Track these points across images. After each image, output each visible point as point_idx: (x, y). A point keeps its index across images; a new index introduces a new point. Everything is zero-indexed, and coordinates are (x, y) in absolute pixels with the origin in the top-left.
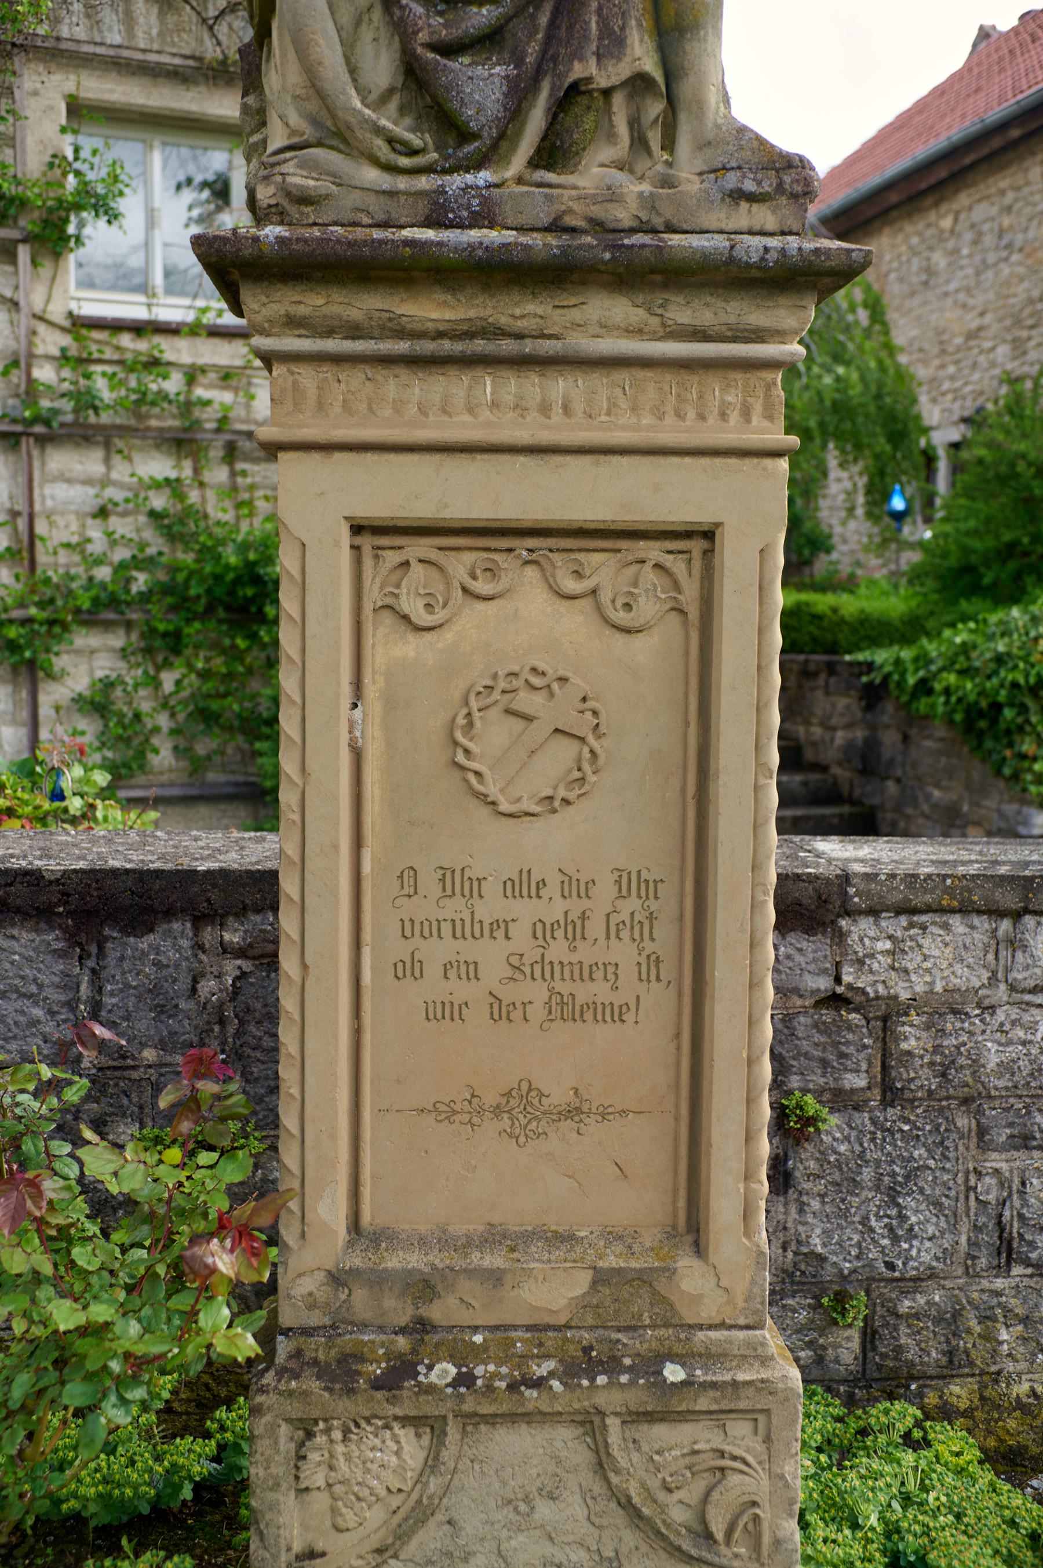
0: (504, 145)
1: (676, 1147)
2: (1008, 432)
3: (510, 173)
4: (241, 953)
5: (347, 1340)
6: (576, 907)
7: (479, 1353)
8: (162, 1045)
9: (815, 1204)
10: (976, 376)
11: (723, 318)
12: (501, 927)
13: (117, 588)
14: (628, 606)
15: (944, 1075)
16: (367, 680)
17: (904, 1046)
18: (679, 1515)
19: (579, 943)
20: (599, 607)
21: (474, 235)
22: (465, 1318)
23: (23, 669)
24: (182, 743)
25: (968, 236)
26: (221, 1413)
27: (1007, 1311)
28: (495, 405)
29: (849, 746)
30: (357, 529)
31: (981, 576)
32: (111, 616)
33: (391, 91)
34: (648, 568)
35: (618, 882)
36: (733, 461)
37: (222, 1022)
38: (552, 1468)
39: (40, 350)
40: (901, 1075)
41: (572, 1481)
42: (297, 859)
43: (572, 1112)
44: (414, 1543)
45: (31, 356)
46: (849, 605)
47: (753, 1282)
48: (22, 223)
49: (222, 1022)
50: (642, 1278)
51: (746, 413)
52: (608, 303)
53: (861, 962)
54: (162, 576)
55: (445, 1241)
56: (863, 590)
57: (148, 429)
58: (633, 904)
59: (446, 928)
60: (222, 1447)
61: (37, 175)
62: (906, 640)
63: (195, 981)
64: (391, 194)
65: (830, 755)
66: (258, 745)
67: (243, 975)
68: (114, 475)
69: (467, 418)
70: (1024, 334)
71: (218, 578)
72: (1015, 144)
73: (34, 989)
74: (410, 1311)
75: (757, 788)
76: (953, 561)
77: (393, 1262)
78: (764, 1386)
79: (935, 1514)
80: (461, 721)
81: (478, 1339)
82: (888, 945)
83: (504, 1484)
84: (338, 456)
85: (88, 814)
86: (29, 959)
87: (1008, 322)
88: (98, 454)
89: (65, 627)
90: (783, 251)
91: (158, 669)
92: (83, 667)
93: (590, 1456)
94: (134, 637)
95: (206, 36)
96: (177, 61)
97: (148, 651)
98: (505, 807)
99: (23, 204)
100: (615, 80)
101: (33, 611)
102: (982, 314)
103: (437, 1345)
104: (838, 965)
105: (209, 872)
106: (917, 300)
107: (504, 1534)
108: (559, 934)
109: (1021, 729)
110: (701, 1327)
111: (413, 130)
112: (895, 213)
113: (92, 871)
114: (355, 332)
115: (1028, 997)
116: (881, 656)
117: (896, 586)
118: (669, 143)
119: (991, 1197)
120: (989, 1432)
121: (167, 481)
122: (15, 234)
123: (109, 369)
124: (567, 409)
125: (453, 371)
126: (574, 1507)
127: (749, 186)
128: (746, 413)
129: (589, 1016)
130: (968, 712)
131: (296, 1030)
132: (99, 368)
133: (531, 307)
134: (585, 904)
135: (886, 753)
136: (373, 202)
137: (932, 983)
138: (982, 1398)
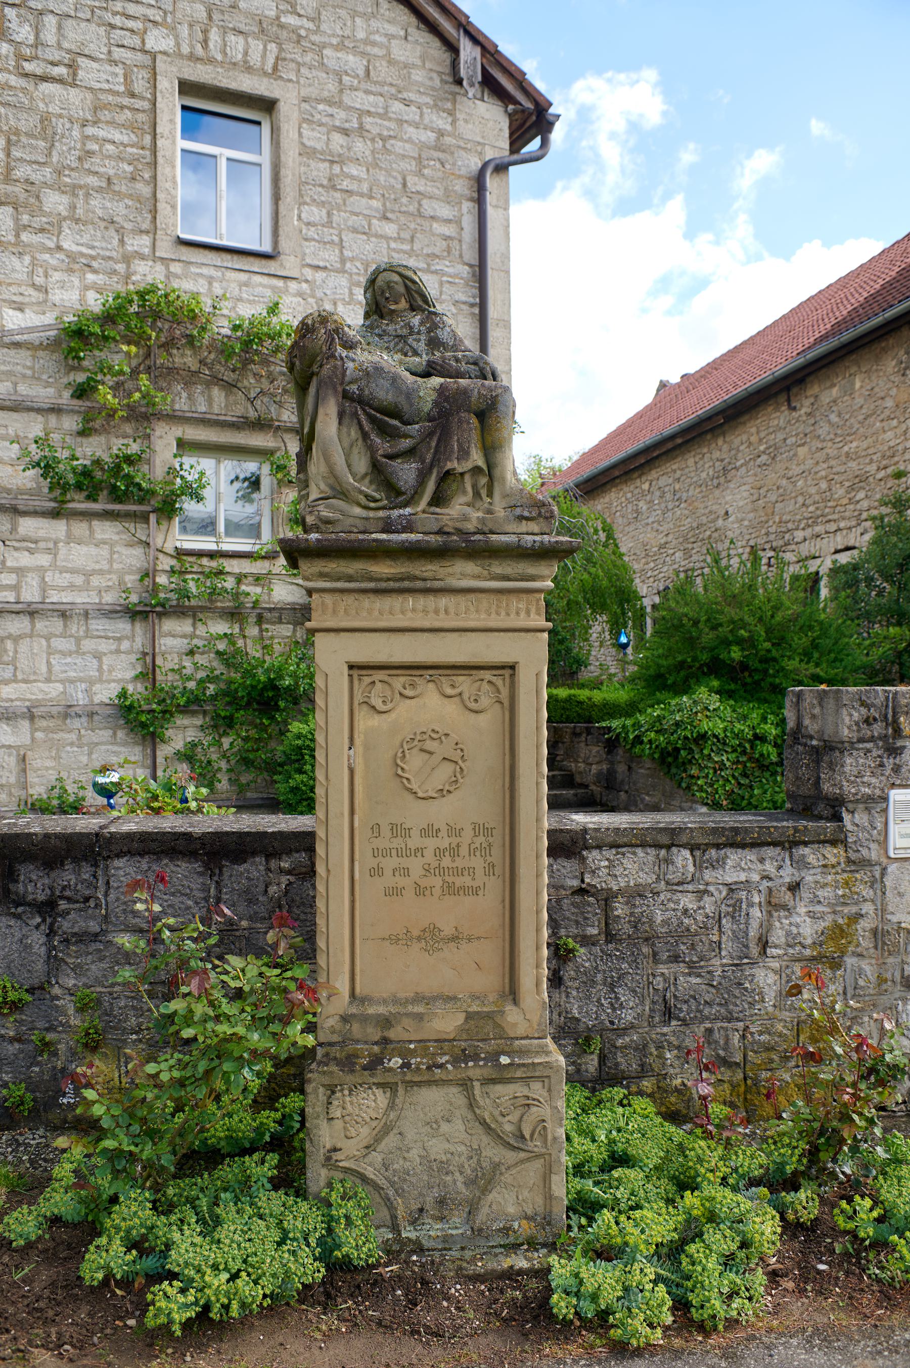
0: (417, 496)
1: (504, 954)
2: (678, 602)
3: (419, 509)
4: (289, 872)
5: (350, 1048)
6: (455, 841)
7: (413, 1053)
8: (250, 919)
9: (574, 993)
10: (665, 569)
11: (516, 571)
12: (419, 851)
13: (199, 693)
14: (476, 701)
15: (636, 927)
16: (356, 736)
17: (616, 913)
18: (508, 1128)
19: (456, 858)
20: (463, 701)
21: (404, 536)
22: (406, 1036)
23: (148, 738)
24: (234, 777)
25: (658, 493)
26: (282, 1100)
27: (669, 1043)
28: (414, 610)
29: (600, 773)
30: (351, 667)
31: (667, 679)
32: (196, 708)
33: (366, 475)
34: (485, 683)
35: (474, 829)
36: (523, 634)
37: (280, 907)
38: (448, 1107)
39: (159, 568)
40: (615, 927)
41: (457, 1113)
42: (324, 819)
43: (454, 939)
44: (383, 1143)
45: (155, 570)
46: (598, 696)
47: (541, 1016)
48: (152, 502)
49: (280, 907)
50: (489, 1016)
51: (528, 613)
52: (464, 564)
53: (594, 872)
54: (223, 686)
55: (396, 1001)
56: (604, 688)
57: (216, 607)
58: (481, 839)
59: (394, 852)
60: (284, 1116)
61: (160, 479)
62: (628, 715)
63: (267, 887)
64: (367, 519)
65: (589, 779)
66: (275, 777)
67: (290, 883)
68: (198, 632)
69: (401, 616)
70: (690, 546)
71: (253, 687)
72: (680, 446)
73: (188, 891)
74: (380, 1034)
75: (537, 784)
76: (652, 672)
77: (371, 1011)
78: (548, 1065)
79: (632, 1133)
80: (400, 755)
81: (412, 1046)
82: (607, 863)
83: (426, 1114)
84: (342, 634)
85: (200, 810)
86: (186, 877)
87: (681, 540)
88: (189, 621)
89: (172, 715)
90: (542, 542)
91: (221, 736)
92: (180, 736)
93: (466, 1100)
94: (207, 719)
95: (249, 406)
96: (234, 419)
97: (215, 726)
98: (420, 794)
99: (153, 493)
100: (465, 469)
101: (154, 706)
102: (667, 535)
103: (393, 1049)
104: (582, 873)
105: (273, 833)
106: (632, 527)
107: (426, 1139)
108: (447, 854)
109: (690, 762)
110: (517, 1039)
111: (376, 491)
112: (618, 481)
113: (217, 833)
114: (350, 579)
115: (675, 887)
116: (615, 724)
117: (623, 686)
118: (490, 494)
119: (660, 987)
120: (662, 1104)
121: (225, 634)
122: (149, 508)
123: (196, 577)
124: (446, 612)
125: (394, 595)
126: (459, 1125)
127: (526, 514)
128: (528, 613)
129: (461, 892)
130: (662, 753)
131: (324, 900)
132: (189, 576)
133: (429, 567)
134: (459, 839)
135: (620, 777)
136: (358, 522)
137: (628, 882)
138: (658, 1087)
